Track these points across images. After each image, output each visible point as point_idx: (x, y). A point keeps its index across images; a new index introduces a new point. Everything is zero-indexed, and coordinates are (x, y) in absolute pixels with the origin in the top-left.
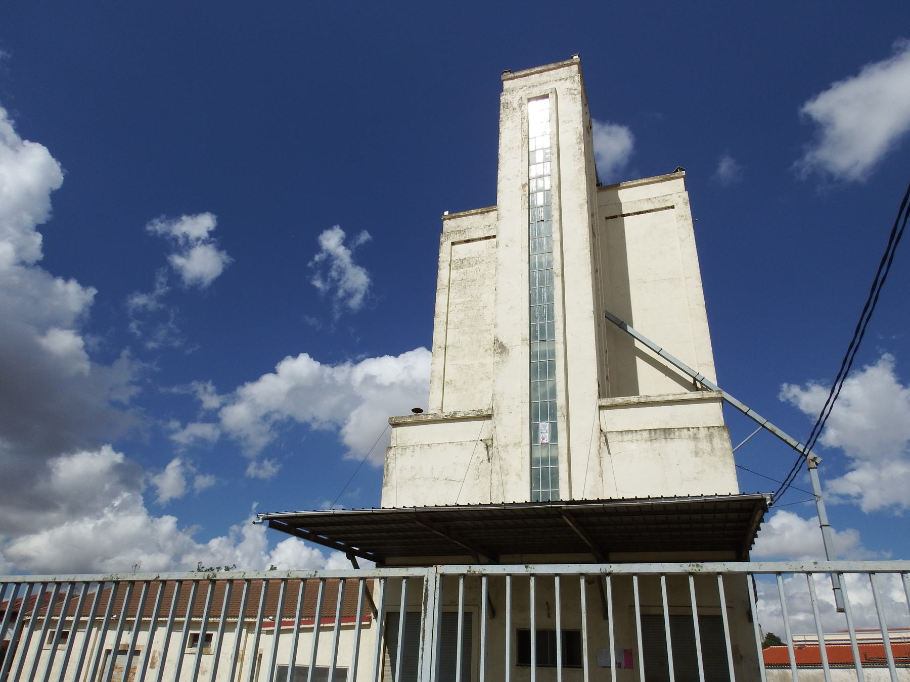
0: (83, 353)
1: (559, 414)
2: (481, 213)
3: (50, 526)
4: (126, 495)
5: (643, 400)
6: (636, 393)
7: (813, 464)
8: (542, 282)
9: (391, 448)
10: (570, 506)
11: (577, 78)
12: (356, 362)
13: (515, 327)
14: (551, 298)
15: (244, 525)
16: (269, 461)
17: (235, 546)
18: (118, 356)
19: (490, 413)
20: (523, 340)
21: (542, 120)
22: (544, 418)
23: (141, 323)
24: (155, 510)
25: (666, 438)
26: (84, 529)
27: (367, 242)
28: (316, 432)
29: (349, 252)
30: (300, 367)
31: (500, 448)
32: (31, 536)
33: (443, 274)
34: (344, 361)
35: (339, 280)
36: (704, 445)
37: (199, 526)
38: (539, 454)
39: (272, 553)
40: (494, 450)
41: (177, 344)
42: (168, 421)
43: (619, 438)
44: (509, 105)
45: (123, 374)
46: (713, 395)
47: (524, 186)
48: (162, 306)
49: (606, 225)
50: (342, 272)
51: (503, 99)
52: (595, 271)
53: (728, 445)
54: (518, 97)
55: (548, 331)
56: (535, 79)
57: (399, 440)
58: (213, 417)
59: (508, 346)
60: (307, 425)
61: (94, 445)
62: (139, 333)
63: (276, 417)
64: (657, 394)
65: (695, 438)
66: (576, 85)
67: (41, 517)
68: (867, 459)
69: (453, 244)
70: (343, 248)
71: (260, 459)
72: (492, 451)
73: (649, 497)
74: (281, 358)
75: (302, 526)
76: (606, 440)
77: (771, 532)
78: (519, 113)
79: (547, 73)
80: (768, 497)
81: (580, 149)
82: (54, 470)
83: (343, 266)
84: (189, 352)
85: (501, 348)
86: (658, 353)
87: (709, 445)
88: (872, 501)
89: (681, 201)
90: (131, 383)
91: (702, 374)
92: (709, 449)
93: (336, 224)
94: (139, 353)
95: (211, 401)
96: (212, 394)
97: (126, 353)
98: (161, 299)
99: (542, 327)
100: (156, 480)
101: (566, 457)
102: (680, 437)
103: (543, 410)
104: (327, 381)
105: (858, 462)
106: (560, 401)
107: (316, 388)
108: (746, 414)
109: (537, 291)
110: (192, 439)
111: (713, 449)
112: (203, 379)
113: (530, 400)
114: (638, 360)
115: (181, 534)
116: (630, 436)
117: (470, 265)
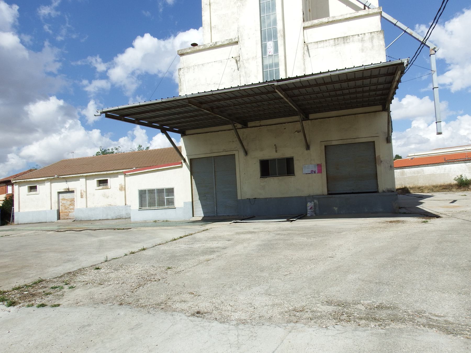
0: (21, 45)
1: (279, 35)
3: (37, 140)
4: (70, 121)
5: (330, 20)
6: (327, 14)
7: (433, 52)
12: (175, 36)
15: (134, 130)
16: (139, 96)
17: (132, 141)
18: (43, 46)
19: (236, 40)
22: (270, 39)
23: (50, 25)
24: (88, 127)
25: (344, 43)
26: (54, 140)
28: (162, 79)
30: (146, 42)
31: (244, 61)
32: (29, 146)
34: (170, 36)
36: (368, 44)
37: (112, 133)
38: (268, 62)
39: (151, 142)
40: (241, 63)
41: (74, 36)
42: (81, 81)
43: (316, 46)
45: (49, 56)
46: (376, 11)
48: (59, 13)
53: (382, 42)
58: (104, 76)
60: (156, 75)
61: (46, 97)
62: (51, 32)
63: (138, 72)
65: (362, 40)
67: (31, 137)
68: (457, 64)
71: (134, 96)
72: (240, 63)
74: (134, 38)
75: (127, 115)
76: (308, 48)
82: (29, 112)
84: (83, 41)
88: (457, 86)
90: (55, 61)
91: (370, 2)
94: (54, 43)
95: (101, 67)
96: (100, 63)
97: (47, 43)
98: (57, 9)
100: (84, 112)
102: (353, 41)
103: (268, 34)
104: (163, 49)
105: (452, 65)
106: (279, 26)
108: (395, 25)
110: (97, 89)
111: (373, 47)
112: (93, 54)
113: (261, 29)
115: (104, 138)
116: (322, 44)
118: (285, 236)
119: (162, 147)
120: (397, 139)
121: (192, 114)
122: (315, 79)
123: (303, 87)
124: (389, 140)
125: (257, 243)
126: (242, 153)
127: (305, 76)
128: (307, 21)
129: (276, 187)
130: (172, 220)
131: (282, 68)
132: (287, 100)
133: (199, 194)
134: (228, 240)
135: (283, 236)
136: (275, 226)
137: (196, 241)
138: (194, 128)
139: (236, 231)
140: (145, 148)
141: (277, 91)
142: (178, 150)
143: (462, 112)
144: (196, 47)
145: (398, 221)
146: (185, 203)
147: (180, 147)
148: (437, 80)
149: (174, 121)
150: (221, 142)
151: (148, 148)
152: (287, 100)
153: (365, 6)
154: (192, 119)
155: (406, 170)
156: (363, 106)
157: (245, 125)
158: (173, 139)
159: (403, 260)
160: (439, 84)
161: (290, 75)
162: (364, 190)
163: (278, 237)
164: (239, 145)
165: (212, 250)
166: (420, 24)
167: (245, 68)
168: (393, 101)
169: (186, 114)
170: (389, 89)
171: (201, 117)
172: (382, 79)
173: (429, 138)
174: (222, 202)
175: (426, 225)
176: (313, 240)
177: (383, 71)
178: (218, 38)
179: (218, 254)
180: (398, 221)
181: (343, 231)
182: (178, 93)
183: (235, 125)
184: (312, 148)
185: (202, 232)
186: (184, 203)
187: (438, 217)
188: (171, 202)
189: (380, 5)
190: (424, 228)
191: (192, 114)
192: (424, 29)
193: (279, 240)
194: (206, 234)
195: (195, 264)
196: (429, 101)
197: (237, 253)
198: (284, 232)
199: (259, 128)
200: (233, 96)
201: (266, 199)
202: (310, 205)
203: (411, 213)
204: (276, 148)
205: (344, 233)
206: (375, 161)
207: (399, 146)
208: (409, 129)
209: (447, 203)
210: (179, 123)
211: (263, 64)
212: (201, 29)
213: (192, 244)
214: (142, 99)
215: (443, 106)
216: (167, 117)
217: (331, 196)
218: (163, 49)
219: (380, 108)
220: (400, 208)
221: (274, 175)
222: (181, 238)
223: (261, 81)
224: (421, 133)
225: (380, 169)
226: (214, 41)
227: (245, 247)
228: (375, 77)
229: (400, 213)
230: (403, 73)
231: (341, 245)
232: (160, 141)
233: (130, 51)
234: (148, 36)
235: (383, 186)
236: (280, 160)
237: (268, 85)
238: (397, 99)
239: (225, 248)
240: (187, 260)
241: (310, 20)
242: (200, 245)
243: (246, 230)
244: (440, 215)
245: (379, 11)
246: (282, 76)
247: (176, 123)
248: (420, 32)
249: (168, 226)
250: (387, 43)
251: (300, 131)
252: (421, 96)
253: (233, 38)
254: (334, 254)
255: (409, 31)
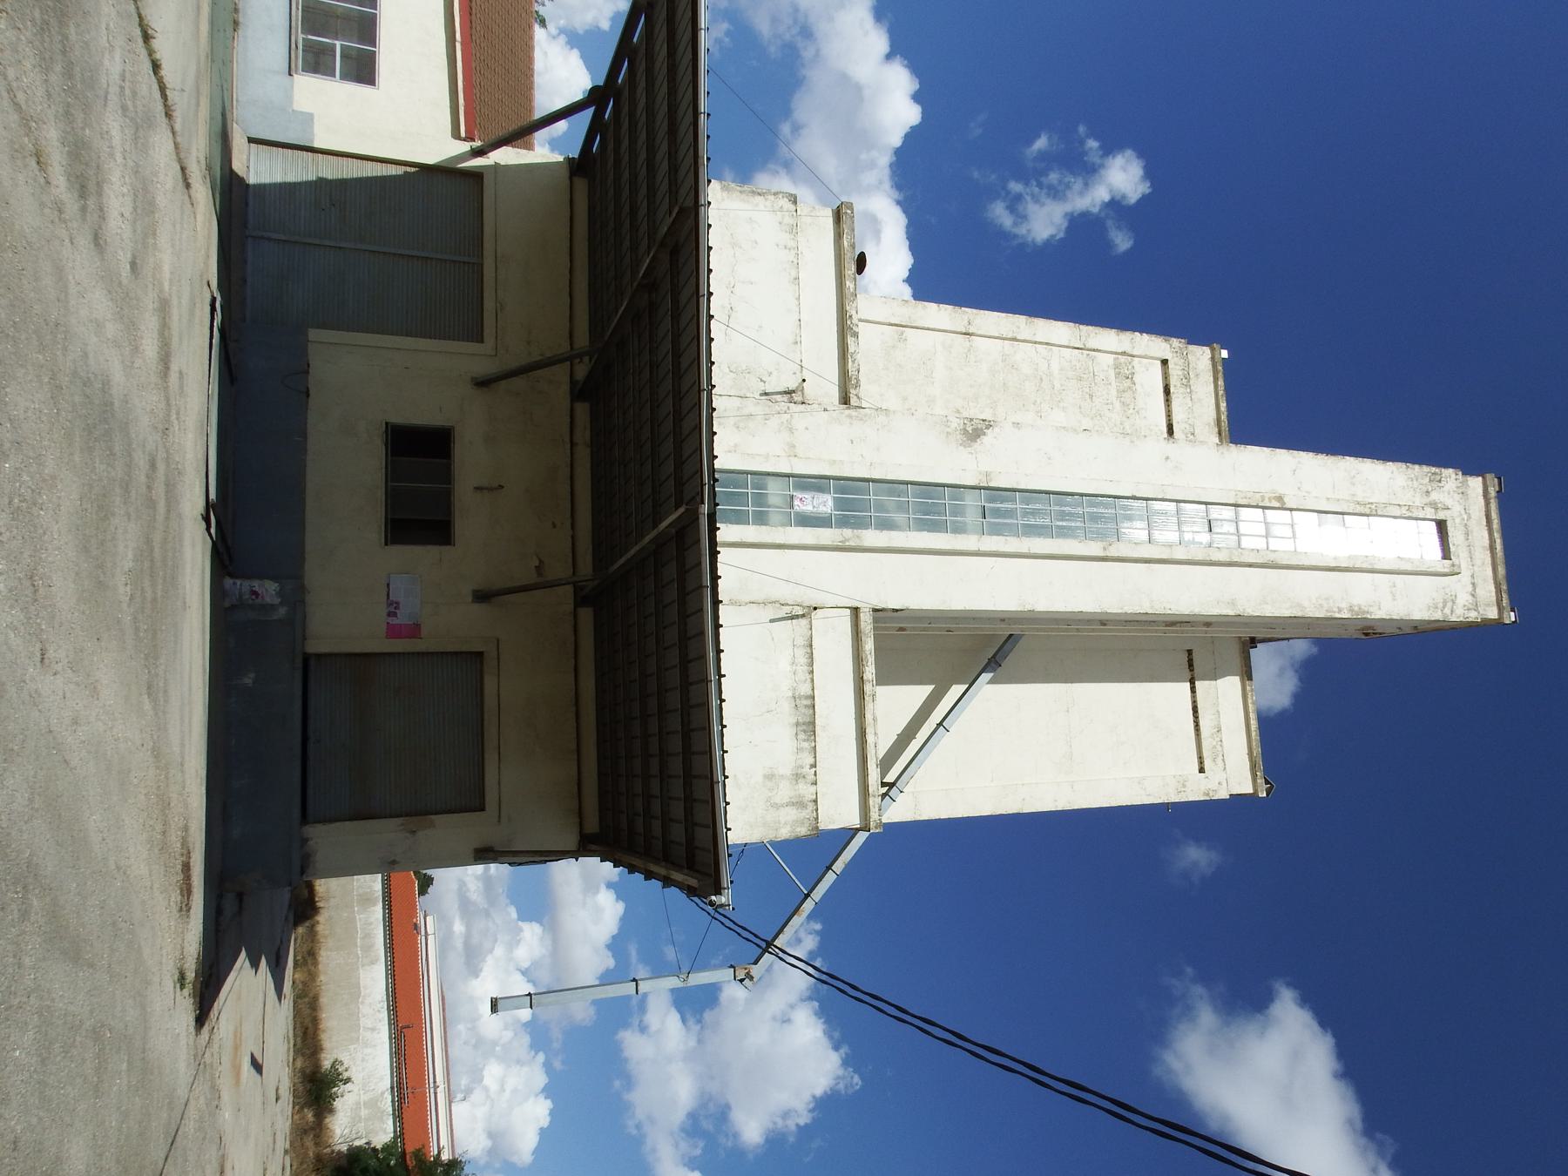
1: (848, 532)
2: (1219, 421)
5: (868, 688)
6: (882, 679)
8: (1095, 518)
9: (795, 202)
10: (704, 522)
11: (1473, 616)
13: (1010, 461)
14: (1064, 533)
16: (728, 33)
19: (854, 401)
20: (987, 474)
21: (1393, 543)
22: (839, 504)
25: (797, 724)
27: (1109, 245)
29: (1095, 210)
30: (896, 105)
33: (1108, 339)
35: (1040, 185)
36: (785, 792)
38: (774, 490)
39: (563, 39)
43: (801, 641)
44: (1435, 485)
46: (874, 815)
47: (1280, 498)
49: (1185, 649)
50: (1056, 193)
51: (1449, 473)
52: (1103, 621)
53: (784, 833)
54: (1449, 503)
55: (1007, 530)
56: (1481, 536)
57: (809, 220)
59: (976, 445)
60: (787, 112)
63: (808, 54)
64: (878, 714)
65: (798, 777)
66: (1461, 613)
68: (700, 1041)
69: (1165, 362)
70: (1107, 198)
73: (721, 676)
74: (915, 68)
76: (797, 617)
77: (590, 888)
78: (1419, 500)
79: (1488, 560)
80: (723, 900)
81: (1340, 610)
83: (1068, 193)
85: (974, 433)
86: (940, 724)
87: (786, 800)
88: (635, 1045)
89: (1212, 785)
91: (900, 798)
92: (778, 800)
93: (1152, 186)
99: (1010, 513)
101: (1024, 550)
102: (799, 750)
103: (856, 502)
104: (864, 156)
106: (872, 537)
107: (854, 136)
108: (829, 868)
109: (1080, 511)
111: (776, 806)
113: (874, 481)
114: (929, 689)
116: (803, 660)
117: (1121, 392)
118: (144, 489)
119: (539, 80)
120: (487, 881)
121: (643, 211)
122: (702, 633)
123: (683, 594)
124: (484, 854)
125: (118, 377)
126: (484, 368)
127: (716, 602)
128: (875, 620)
129: (344, 478)
130: (239, 46)
131: (749, 532)
132: (647, 539)
133: (342, 184)
134: (133, 265)
135: (143, 478)
136: (190, 456)
137: (139, 127)
138: (591, 209)
139: (175, 302)
140: (542, 11)
141: (682, 510)
142: (520, 135)
143: (557, 1064)
144: (854, 268)
145: (187, 891)
146: (308, 119)
147: (529, 147)
148: (659, 990)
149: (626, 143)
150: (532, 299)
151: (543, 23)
152: (647, 539)
153: (891, 785)
154: (627, 208)
155: (378, 911)
156: (601, 775)
157: (579, 393)
158: (561, 126)
159: (25, 915)
160: (645, 995)
161: (724, 556)
162: (312, 777)
163: (141, 460)
164: (513, 363)
165: (92, 186)
166: (822, 934)
167: (767, 417)
168: (609, 865)
169: (643, 191)
170: (647, 854)
171: (627, 243)
172: (678, 833)
173: (483, 974)
174: (292, 263)
175: (169, 983)
176: (123, 591)
177: (702, 835)
178: (868, 343)
179: (72, 206)
180: (187, 891)
181: (155, 701)
182: (720, 179)
183: (586, 359)
184: (479, 609)
185: (180, 160)
186: (311, 116)
187: (201, 1020)
188: (317, 62)
189: (890, 827)
190: (156, 979)
191: (643, 211)
192: (809, 944)
193: (129, 466)
194: (167, 177)
195: (21, 97)
196: (601, 969)
197: (73, 290)
198: (159, 491)
199: (567, 439)
200: (684, 365)
201: (304, 435)
202: (269, 590)
203: (217, 931)
204: (490, 489)
205: (147, 706)
206: (417, 811)
207: (461, 886)
208: (514, 915)
209: (250, 1046)
210: (617, 162)
211: (768, 474)
212: (907, 291)
213: (124, 108)
214: (718, 41)
215: (581, 1010)
216: (644, 118)
217: (299, 662)
218: (864, 156)
219: (592, 825)
220: (240, 896)
221: (393, 473)
222: (156, 66)
223: (718, 464)
224: (499, 951)
225: (387, 831)
226: (862, 329)
227: (99, 325)
228: (689, 812)
229: (220, 896)
230: (691, 892)
231: (94, 691)
232: (562, 75)
233: (878, 42)
234: (910, 114)
235: (322, 837)
236: (445, 500)
237: (703, 485)
238: (616, 879)
239: (98, 240)
240: (45, 66)
241: (875, 629)
242: (117, 141)
243: (175, 340)
244: (206, 1028)
245: (872, 825)
246: (725, 532)
247: (617, 151)
248: (801, 936)
249: (212, 23)
250: (782, 846)
251: (540, 574)
252: (616, 945)
253: (862, 391)
254: (59, 667)
255: (808, 906)
